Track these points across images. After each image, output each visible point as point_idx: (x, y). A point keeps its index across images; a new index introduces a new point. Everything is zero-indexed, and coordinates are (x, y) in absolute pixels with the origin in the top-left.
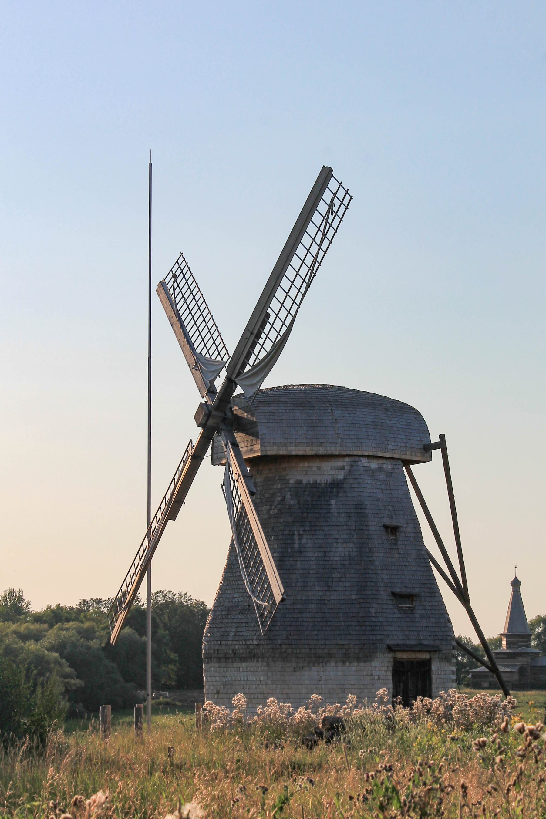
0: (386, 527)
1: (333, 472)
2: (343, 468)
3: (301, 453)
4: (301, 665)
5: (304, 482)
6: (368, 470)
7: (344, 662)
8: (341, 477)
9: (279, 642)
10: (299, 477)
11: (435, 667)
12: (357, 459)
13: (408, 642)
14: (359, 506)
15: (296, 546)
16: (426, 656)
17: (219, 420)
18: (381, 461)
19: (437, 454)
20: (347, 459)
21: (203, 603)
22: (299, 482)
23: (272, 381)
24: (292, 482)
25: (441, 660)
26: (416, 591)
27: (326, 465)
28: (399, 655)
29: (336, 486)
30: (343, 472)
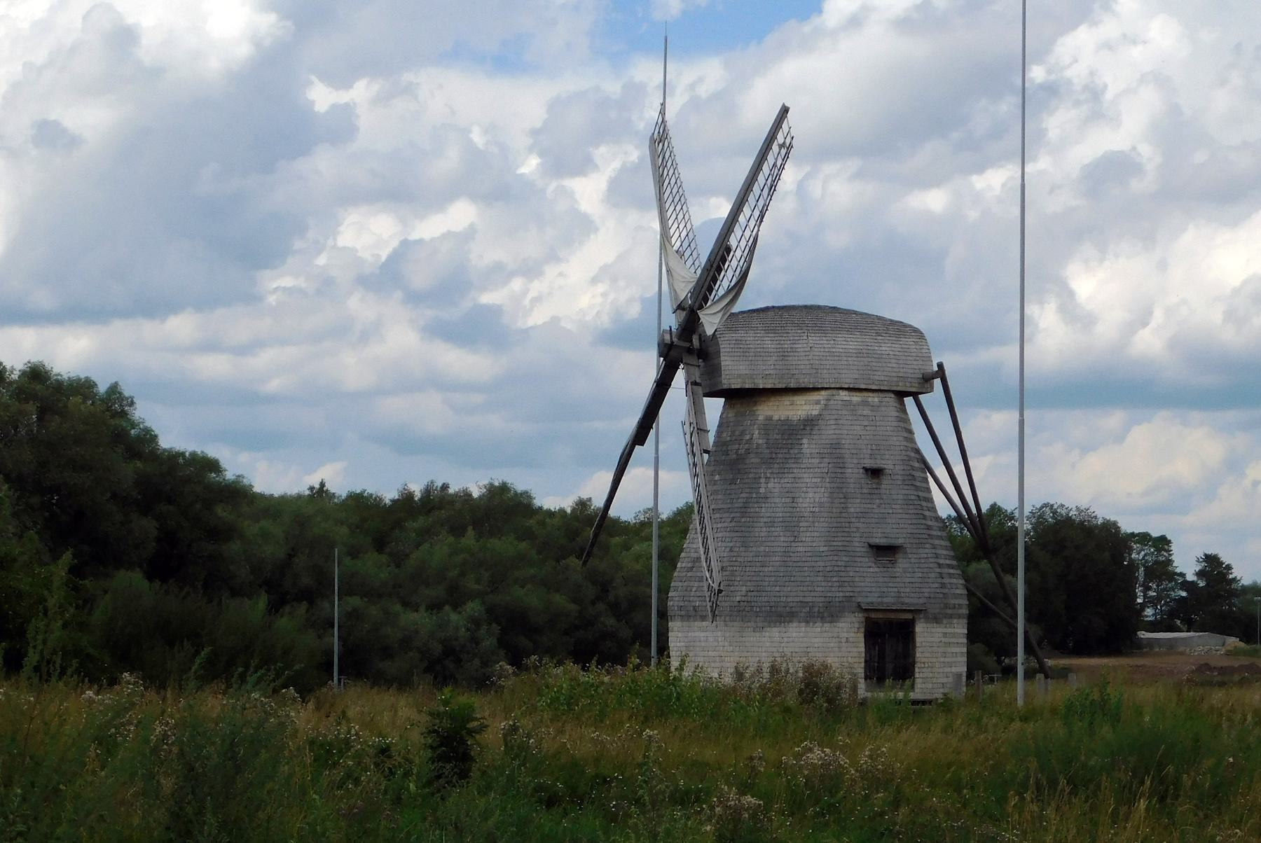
0: (866, 470)
1: (807, 407)
2: (818, 403)
3: (769, 386)
4: (760, 624)
5: (776, 418)
6: (847, 404)
7: (807, 622)
8: (815, 413)
9: (738, 599)
10: (769, 413)
11: (920, 628)
12: (834, 392)
13: (885, 600)
14: (836, 446)
15: (762, 490)
16: (909, 616)
17: (686, 348)
18: (866, 394)
19: (937, 383)
20: (823, 393)
21: (1115, 523)
22: (769, 419)
23: (747, 301)
24: (761, 418)
25: (927, 620)
26: (900, 541)
27: (800, 400)
28: (873, 615)
29: (809, 424)
30: (818, 407)
